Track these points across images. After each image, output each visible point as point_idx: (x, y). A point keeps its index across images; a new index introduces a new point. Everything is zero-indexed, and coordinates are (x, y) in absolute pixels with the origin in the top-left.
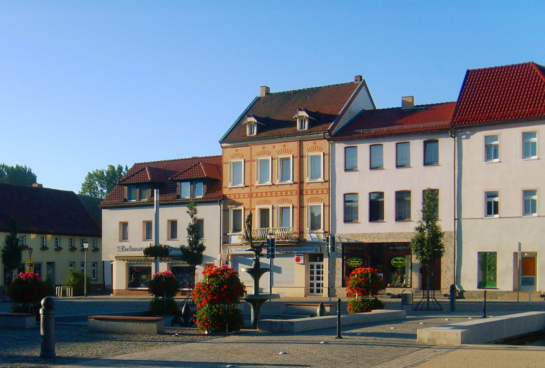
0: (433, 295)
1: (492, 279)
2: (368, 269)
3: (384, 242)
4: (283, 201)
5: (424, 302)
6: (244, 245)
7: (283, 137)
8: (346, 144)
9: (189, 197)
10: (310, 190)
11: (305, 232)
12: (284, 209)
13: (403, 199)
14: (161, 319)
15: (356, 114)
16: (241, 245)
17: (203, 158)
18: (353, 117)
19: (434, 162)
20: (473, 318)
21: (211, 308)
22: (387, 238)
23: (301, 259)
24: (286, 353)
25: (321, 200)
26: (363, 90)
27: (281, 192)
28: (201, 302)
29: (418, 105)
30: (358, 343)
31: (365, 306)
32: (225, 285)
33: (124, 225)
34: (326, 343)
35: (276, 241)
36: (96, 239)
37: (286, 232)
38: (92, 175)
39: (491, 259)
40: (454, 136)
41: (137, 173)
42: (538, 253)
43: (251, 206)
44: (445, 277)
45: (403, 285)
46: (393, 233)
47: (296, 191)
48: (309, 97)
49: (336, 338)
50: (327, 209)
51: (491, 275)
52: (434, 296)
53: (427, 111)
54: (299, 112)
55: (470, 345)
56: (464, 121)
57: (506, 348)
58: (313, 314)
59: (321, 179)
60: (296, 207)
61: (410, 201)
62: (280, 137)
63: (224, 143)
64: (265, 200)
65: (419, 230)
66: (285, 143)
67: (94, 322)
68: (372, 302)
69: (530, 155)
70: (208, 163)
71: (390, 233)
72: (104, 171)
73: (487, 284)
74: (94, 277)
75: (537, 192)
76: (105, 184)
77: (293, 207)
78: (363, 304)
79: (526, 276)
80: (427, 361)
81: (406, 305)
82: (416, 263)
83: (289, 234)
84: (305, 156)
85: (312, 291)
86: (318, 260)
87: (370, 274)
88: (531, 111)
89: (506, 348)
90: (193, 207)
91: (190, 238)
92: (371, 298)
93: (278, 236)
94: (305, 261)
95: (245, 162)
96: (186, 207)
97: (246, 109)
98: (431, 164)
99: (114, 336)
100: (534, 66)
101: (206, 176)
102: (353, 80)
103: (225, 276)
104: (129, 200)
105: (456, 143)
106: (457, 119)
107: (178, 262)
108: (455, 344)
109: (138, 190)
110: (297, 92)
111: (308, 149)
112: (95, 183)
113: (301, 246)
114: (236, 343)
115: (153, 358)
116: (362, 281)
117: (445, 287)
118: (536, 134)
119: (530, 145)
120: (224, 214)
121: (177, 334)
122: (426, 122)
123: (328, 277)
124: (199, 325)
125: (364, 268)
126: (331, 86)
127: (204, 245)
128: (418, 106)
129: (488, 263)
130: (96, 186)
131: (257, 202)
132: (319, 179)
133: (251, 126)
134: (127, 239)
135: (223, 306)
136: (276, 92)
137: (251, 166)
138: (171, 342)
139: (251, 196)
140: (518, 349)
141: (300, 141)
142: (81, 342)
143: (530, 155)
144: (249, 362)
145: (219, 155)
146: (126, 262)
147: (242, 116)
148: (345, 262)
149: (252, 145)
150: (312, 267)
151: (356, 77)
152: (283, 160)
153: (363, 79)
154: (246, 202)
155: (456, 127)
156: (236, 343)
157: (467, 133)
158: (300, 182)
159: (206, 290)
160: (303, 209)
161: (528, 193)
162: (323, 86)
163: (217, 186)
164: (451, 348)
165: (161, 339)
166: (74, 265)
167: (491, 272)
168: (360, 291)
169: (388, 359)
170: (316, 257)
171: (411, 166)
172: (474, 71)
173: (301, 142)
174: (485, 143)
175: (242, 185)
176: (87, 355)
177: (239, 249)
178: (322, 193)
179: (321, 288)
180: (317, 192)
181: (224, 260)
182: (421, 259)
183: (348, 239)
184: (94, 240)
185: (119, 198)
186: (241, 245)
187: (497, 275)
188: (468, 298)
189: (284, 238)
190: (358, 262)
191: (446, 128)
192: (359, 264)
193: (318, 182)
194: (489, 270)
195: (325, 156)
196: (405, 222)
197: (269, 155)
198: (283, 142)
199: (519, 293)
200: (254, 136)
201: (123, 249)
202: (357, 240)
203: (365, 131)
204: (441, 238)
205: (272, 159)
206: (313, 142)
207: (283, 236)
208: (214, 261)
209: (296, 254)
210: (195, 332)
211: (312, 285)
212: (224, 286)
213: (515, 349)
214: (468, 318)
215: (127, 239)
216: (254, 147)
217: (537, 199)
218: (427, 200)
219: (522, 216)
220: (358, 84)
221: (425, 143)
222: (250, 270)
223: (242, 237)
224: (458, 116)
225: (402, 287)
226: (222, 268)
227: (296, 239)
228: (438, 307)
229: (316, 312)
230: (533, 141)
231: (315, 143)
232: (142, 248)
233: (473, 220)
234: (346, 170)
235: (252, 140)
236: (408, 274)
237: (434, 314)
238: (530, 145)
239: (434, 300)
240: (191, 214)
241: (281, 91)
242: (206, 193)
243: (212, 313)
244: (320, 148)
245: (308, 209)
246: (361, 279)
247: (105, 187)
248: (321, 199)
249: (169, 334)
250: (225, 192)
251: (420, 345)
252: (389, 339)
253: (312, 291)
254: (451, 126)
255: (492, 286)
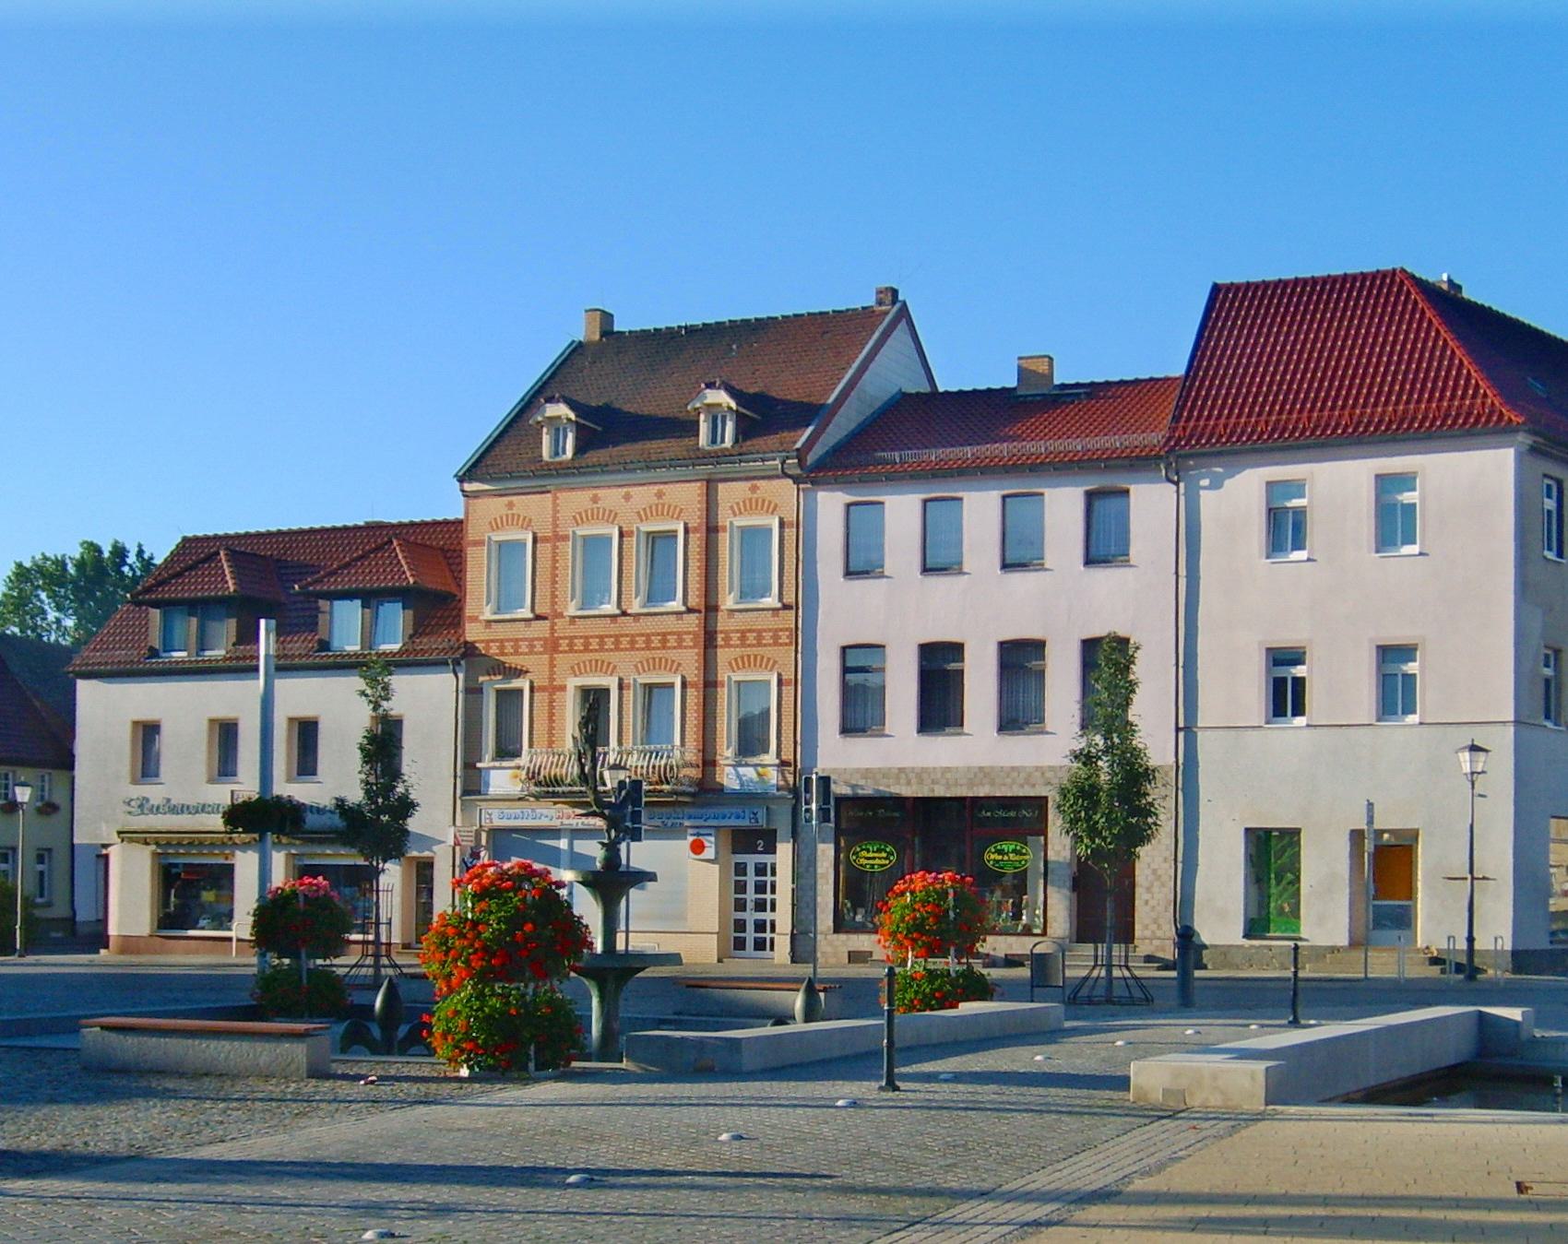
0: (1123, 959)
1: (1287, 909)
2: (946, 876)
3: (964, 795)
4: (655, 665)
5: (1098, 978)
6: (532, 799)
7: (655, 468)
8: (848, 494)
9: (357, 648)
10: (738, 631)
11: (721, 762)
12: (655, 690)
13: (1023, 667)
14: (321, 1028)
15: (878, 404)
16: (520, 799)
17: (401, 525)
18: (868, 412)
19: (1113, 556)
20: (1262, 1026)
21: (481, 996)
22: (971, 784)
23: (706, 844)
24: (742, 1138)
25: (770, 664)
26: (901, 332)
27: (648, 636)
28: (451, 974)
29: (1067, 382)
30: (952, 1104)
31: (936, 990)
32: (526, 922)
33: (148, 732)
34: (854, 1104)
35: (645, 787)
36: (50, 774)
37: (663, 762)
38: (28, 570)
39: (1283, 850)
40: (1176, 478)
41: (190, 568)
42: (1420, 832)
43: (552, 679)
44: (1147, 902)
45: (1020, 928)
46: (992, 768)
47: (694, 633)
48: (734, 347)
49: (881, 1088)
50: (788, 691)
51: (1285, 896)
52: (1127, 961)
53: (1093, 402)
54: (708, 391)
55: (1293, 1109)
56: (1195, 438)
57: (1391, 1115)
58: (781, 1020)
59: (771, 601)
60: (694, 685)
61: (1044, 671)
62: (648, 468)
63: (471, 480)
64: (597, 661)
65: (1084, 759)
66: (662, 487)
67: (100, 1039)
68: (958, 977)
69: (1399, 543)
70: (419, 541)
71: (981, 769)
72: (68, 561)
73: (1272, 925)
74: (42, 896)
75: (1418, 653)
76: (71, 601)
77: (684, 685)
78: (931, 982)
79: (1391, 903)
80: (1182, 1158)
81: (1043, 986)
82: (1061, 860)
83: (672, 768)
84: (724, 529)
85: (740, 944)
86: (760, 849)
87: (951, 891)
88: (1400, 413)
89: (1391, 1115)
90: (380, 678)
91: (368, 775)
92: (949, 964)
93: (636, 772)
94: (721, 853)
95: (535, 541)
96: (357, 678)
97: (541, 379)
98: (1109, 562)
99: (170, 1084)
100: (1406, 282)
101: (411, 580)
102: (871, 301)
103: (526, 896)
104: (165, 651)
105: (1182, 498)
106: (1184, 429)
107: (319, 852)
108: (1245, 1107)
109: (194, 621)
110: (696, 331)
111: (732, 508)
112: (37, 596)
113: (702, 806)
114: (572, 1105)
115: (321, 1154)
116: (927, 912)
117: (1148, 933)
118: (1415, 478)
119: (1399, 512)
120: (466, 700)
121: (374, 1078)
122: (1083, 435)
123: (790, 901)
124: (443, 1051)
125: (933, 874)
126: (803, 315)
127: (411, 797)
128: (1064, 386)
129: (1276, 862)
130: (43, 609)
131: (572, 668)
132: (764, 600)
133: (557, 430)
134: (235, 775)
135: (518, 989)
136: (633, 329)
137: (554, 555)
138: (359, 1102)
139: (552, 646)
140: (1435, 1118)
141: (708, 481)
142: (64, 1102)
143: (1399, 543)
144: (635, 1167)
145: (451, 517)
146: (153, 847)
147: (526, 399)
148: (842, 856)
149: (561, 490)
150: (741, 869)
151: (879, 292)
152: (653, 537)
153: (901, 297)
154: (537, 665)
155: (1182, 452)
156: (572, 1105)
157: (1215, 472)
158: (706, 608)
159: (464, 936)
160: (716, 692)
161: (1392, 655)
162: (778, 314)
163: (446, 614)
164: (1238, 1120)
165: (325, 1094)
166: (50, 858)
167: (1285, 889)
168: (920, 943)
169: (1064, 1152)
170: (753, 839)
171: (1047, 566)
172: (1234, 288)
173: (710, 484)
174: (1268, 503)
175: (526, 613)
176: (100, 1144)
177: (511, 811)
178: (776, 644)
179: (768, 935)
180: (759, 638)
181: (466, 846)
182: (1087, 847)
183: (853, 787)
184: (43, 777)
185: (133, 646)
186: (520, 799)
187: (1302, 898)
188: (1215, 969)
189: (655, 778)
190: (884, 855)
191: (1153, 453)
192: (887, 862)
193: (763, 610)
194: (1278, 884)
195: (787, 530)
196: (1028, 734)
197: (612, 523)
198: (656, 483)
199: (1369, 954)
200: (568, 462)
201: (143, 806)
202: (881, 788)
203: (908, 454)
204: (1148, 787)
205: (621, 535)
206: (749, 484)
207: (653, 773)
208: (435, 848)
209: (690, 831)
210: (426, 1072)
211: (740, 926)
212: (523, 926)
213: (1429, 1118)
214: (1248, 1025)
215: (235, 775)
216: (563, 496)
217: (1417, 672)
218: (1106, 669)
219: (1374, 722)
220: (886, 313)
221: (1091, 497)
222: (590, 877)
223: (524, 776)
224: (1188, 420)
225: (1018, 934)
226: (516, 870)
227: (692, 782)
228: (1137, 994)
229: (793, 1009)
230: (1405, 502)
231: (754, 489)
232: (204, 806)
233: (1233, 732)
234: (849, 573)
235: (559, 475)
236: (1036, 895)
237: (1130, 1016)
238: (1399, 512)
239: (1127, 974)
240: (373, 699)
241: (650, 327)
242: (411, 637)
243: (483, 1011)
244: (770, 503)
245: (729, 690)
246: (924, 907)
247: (70, 611)
248: (771, 662)
249: (345, 1077)
250: (473, 633)
251: (1142, 1108)
252: (1042, 1091)
253: (740, 944)
254: (1166, 449)
255: (1286, 930)
